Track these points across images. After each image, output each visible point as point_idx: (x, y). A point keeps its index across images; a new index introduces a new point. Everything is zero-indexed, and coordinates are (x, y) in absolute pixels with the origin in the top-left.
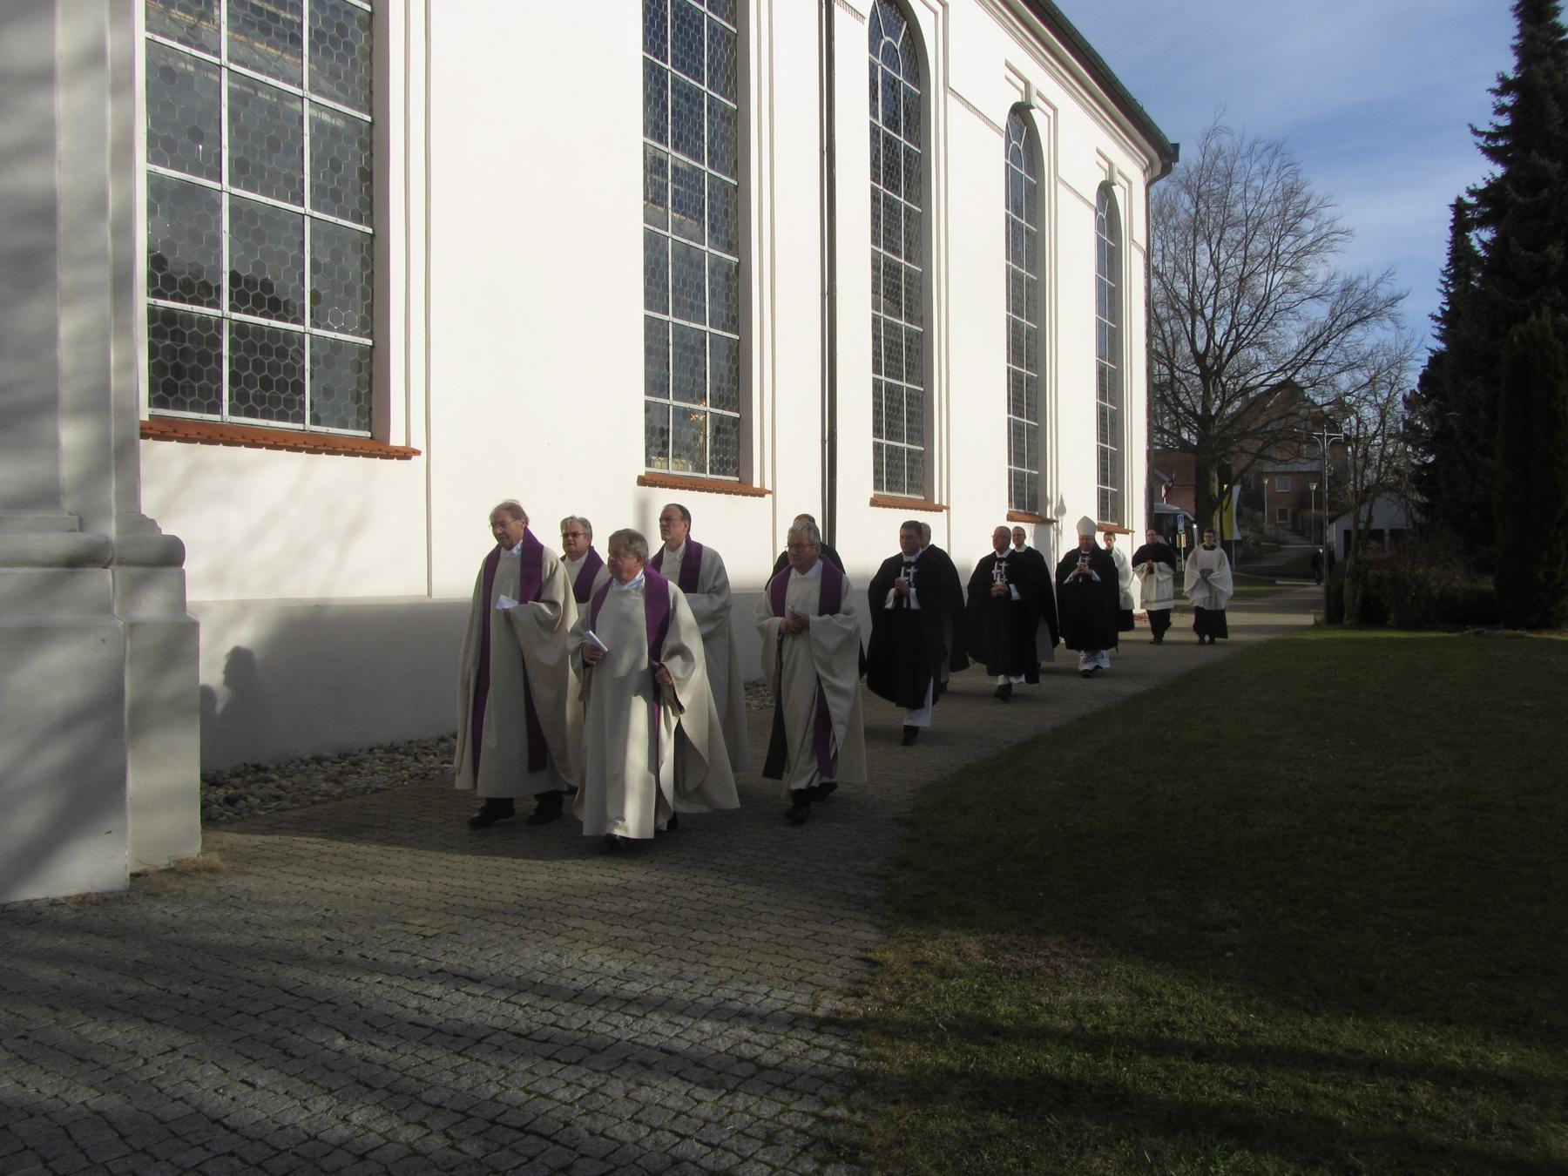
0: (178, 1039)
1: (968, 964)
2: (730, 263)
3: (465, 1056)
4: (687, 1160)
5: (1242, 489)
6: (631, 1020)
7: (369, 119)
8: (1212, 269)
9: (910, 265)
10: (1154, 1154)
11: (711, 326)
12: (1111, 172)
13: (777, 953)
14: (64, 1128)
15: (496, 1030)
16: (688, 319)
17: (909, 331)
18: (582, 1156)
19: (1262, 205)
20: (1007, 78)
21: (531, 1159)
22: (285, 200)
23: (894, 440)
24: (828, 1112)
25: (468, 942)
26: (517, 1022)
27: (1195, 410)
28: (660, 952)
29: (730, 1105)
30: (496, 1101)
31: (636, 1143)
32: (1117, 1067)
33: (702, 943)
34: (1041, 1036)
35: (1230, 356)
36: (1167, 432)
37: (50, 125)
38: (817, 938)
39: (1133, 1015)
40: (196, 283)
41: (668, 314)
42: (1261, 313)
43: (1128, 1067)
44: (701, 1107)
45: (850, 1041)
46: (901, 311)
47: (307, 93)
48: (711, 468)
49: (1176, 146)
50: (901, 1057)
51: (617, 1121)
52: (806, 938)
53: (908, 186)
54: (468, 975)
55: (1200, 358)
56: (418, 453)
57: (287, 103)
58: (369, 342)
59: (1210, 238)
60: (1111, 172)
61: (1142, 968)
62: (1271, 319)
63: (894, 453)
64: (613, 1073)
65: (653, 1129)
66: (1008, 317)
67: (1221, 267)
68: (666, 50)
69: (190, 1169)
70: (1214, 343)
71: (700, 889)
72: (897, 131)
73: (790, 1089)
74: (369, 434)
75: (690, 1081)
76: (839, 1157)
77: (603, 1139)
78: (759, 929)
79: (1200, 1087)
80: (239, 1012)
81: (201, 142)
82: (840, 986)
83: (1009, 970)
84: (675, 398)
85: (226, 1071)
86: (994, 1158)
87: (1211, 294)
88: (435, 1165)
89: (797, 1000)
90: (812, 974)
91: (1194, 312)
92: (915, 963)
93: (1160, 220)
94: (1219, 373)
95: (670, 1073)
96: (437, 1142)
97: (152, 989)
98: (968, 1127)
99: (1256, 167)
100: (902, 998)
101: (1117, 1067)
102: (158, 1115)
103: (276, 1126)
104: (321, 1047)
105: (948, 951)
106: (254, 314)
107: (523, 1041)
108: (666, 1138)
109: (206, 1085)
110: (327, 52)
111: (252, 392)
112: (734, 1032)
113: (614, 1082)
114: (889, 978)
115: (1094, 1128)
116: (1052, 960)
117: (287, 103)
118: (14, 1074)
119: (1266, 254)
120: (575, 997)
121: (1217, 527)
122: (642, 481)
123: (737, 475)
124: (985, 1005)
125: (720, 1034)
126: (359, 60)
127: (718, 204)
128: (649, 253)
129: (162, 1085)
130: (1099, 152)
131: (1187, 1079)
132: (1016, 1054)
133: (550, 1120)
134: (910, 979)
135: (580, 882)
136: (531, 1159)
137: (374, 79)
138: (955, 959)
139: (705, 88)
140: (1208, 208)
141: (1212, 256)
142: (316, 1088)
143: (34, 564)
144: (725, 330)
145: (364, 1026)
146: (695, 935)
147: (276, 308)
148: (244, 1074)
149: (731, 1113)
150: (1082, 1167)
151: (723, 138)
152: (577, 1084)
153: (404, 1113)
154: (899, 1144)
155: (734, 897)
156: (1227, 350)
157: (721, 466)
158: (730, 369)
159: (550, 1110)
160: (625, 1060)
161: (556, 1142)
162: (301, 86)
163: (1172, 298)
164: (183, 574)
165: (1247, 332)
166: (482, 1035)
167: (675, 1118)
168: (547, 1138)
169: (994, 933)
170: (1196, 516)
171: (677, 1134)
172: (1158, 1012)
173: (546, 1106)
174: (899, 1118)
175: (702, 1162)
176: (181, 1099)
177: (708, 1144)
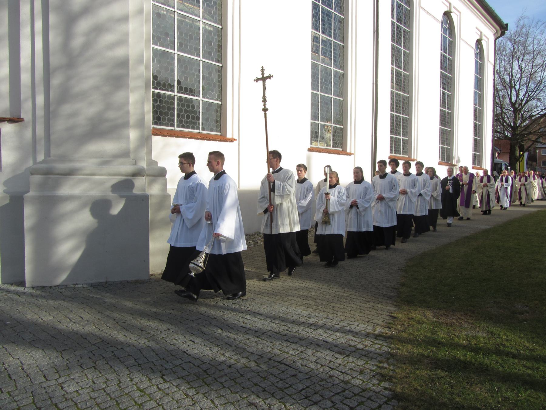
0: (170, 327)
1: (428, 320)
2: (340, 73)
3: (259, 338)
4: (334, 376)
5: (528, 154)
6: (312, 330)
7: (221, 27)
8: (519, 70)
9: (405, 72)
10: (498, 388)
11: (334, 95)
12: (481, 36)
13: (360, 312)
14: (139, 350)
15: (268, 331)
16: (326, 93)
17: (404, 96)
18: (300, 372)
19: (540, 46)
20: (476, 32)
21: (283, 372)
22: (194, 56)
23: (398, 136)
24: (381, 365)
25: (257, 302)
26: (275, 328)
27: (511, 124)
28: (320, 309)
29: (348, 360)
30: (270, 353)
31: (317, 370)
32: (484, 358)
33: (334, 307)
34: (455, 346)
35: (525, 103)
36: (499, 132)
37: (127, 34)
38: (374, 308)
39: (489, 341)
40: (167, 84)
41: (319, 91)
42: (539, 87)
43: (488, 358)
44: (338, 360)
45: (387, 342)
46: (401, 89)
47: (201, 19)
48: (333, 145)
49: (507, 25)
50: (405, 350)
51: (310, 362)
52: (370, 308)
53: (405, 43)
54: (258, 312)
55: (513, 104)
56: (235, 140)
57: (194, 23)
58: (220, 103)
59: (519, 59)
60: (481, 36)
61: (492, 325)
62: (542, 90)
63: (397, 140)
64: (308, 347)
65: (322, 366)
66: (441, 90)
67: (523, 70)
68: (332, 5)
69: (178, 366)
70: (519, 99)
71: (332, 289)
72: (401, 24)
73: (368, 357)
74: (220, 134)
75: (333, 351)
76: (385, 379)
77: (306, 367)
78: (353, 304)
79: (515, 367)
80: (187, 319)
81: (168, 37)
82: (383, 324)
83: (443, 323)
84: (321, 121)
85: (185, 337)
86: (440, 385)
87: (518, 80)
88: (253, 371)
89: (368, 328)
90: (373, 320)
91: (511, 87)
92: (409, 318)
93: (499, 53)
94: (520, 110)
95: (327, 348)
96: (253, 365)
97: (160, 311)
98: (430, 373)
99: (538, 31)
100: (405, 329)
101: (484, 358)
102: (167, 348)
103: (202, 355)
104: (213, 332)
105: (421, 315)
106: (185, 94)
107: (277, 334)
108: (327, 369)
109: (180, 341)
110: (208, 5)
111: (184, 120)
112: (348, 337)
113: (308, 350)
114: (400, 323)
115: (476, 378)
116: (459, 320)
117: (194, 23)
118: (123, 333)
119: (541, 64)
120: (293, 322)
121: (518, 168)
122: (309, 150)
123: (342, 148)
124: (435, 334)
125: (343, 337)
126: (218, 7)
127: (336, 52)
128: (313, 70)
129: (167, 340)
130: (477, 28)
131: (510, 364)
132: (447, 351)
133: (288, 360)
134: (407, 323)
135: (292, 285)
136: (283, 372)
137: (223, 14)
138: (423, 318)
139: (333, 11)
140: (518, 47)
141: (519, 66)
142: (213, 345)
143: (122, 175)
144: (338, 97)
145: (226, 326)
146: (331, 304)
147: (191, 92)
148: (191, 339)
149: (348, 363)
150: (472, 390)
151: (339, 29)
152: (296, 350)
153: (242, 354)
154: (407, 377)
155: (344, 293)
156: (524, 101)
157: (336, 144)
158: (340, 111)
159: (288, 357)
160: (311, 343)
161: (291, 367)
162: (199, 17)
163: (503, 82)
164: (166, 179)
165: (532, 94)
166: (264, 332)
167: (329, 363)
168: (288, 366)
169: (437, 310)
170: (509, 164)
171: (330, 368)
172: (498, 341)
173: (287, 355)
174: (406, 369)
175: (339, 377)
176: (173, 344)
177: (341, 372)
